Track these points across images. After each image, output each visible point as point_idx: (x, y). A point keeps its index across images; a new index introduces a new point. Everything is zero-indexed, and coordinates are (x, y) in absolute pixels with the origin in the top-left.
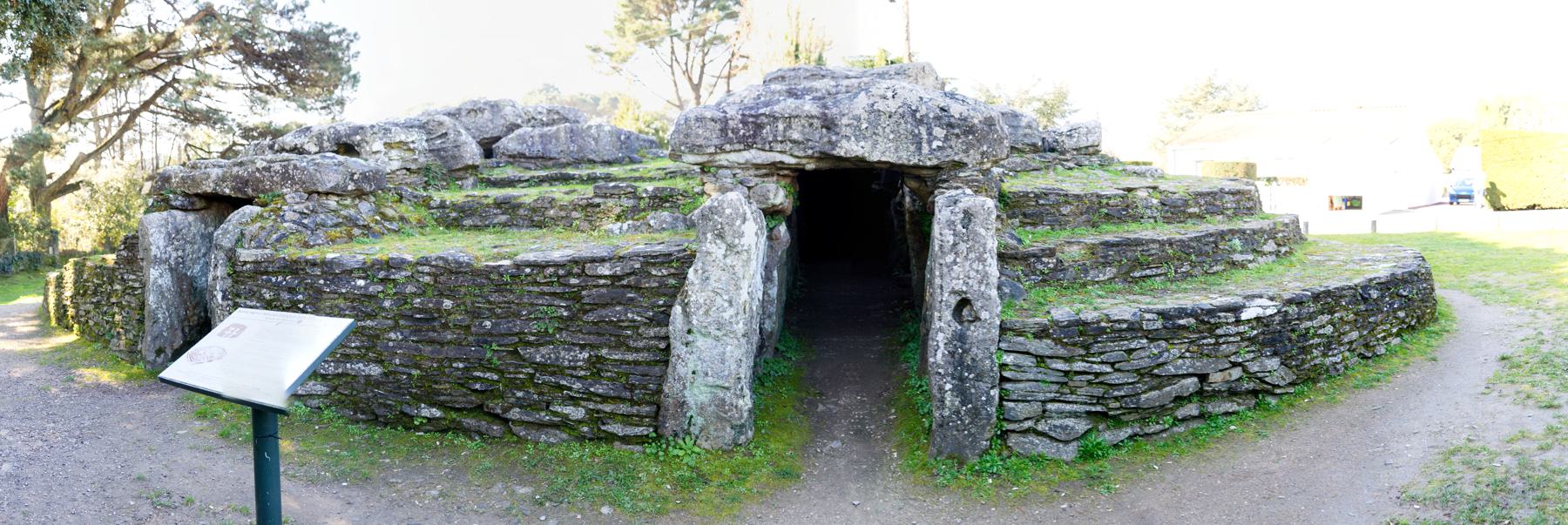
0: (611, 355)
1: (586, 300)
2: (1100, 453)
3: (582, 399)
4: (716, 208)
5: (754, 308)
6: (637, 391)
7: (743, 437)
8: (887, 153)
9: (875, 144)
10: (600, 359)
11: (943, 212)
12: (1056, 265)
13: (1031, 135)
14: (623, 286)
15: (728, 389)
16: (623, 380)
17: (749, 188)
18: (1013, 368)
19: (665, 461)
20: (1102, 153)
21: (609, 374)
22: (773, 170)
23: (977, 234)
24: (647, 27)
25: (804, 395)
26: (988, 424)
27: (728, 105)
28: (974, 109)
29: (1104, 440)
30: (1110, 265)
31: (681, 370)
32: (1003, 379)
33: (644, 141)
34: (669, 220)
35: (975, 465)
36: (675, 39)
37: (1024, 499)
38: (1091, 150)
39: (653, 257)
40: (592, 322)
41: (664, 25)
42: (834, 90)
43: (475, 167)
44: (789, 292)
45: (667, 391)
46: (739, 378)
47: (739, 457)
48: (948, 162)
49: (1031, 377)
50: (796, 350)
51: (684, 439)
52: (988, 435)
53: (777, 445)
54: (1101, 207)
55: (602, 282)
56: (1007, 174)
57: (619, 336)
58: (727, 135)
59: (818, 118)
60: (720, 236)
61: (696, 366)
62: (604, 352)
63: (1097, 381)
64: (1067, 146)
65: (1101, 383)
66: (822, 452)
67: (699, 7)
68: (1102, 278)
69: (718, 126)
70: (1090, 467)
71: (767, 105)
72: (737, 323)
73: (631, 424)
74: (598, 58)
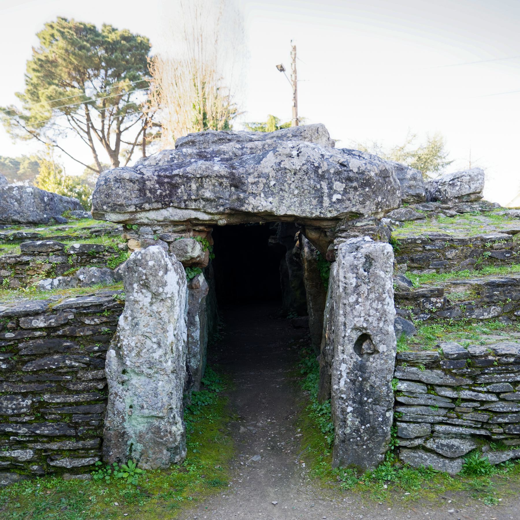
0: (53, 399)
1: (24, 352)
2: (483, 470)
3: (29, 441)
4: (140, 260)
5: (180, 348)
6: (81, 428)
7: (178, 457)
8: (293, 208)
9: (282, 199)
10: (42, 404)
11: (347, 258)
12: (443, 305)
13: (415, 187)
14: (59, 336)
15: (162, 418)
16: (67, 420)
17: (169, 243)
18: (406, 394)
19: (111, 483)
20: (483, 199)
21: (53, 416)
22: (190, 227)
23: (377, 276)
24: (60, 93)
25: (228, 420)
26: (384, 440)
27: (145, 167)
28: (371, 163)
29: (487, 460)
30: (494, 303)
31: (119, 405)
32: (398, 404)
33: (68, 202)
34: (97, 274)
35: (372, 473)
36: (90, 107)
37: (415, 503)
38: (473, 197)
39: (85, 308)
40: (32, 371)
41: (77, 92)
42: (240, 152)
44: (209, 334)
45: (108, 424)
46: (171, 408)
47: (175, 474)
48: (346, 213)
49: (422, 402)
50: (219, 384)
51: (127, 464)
52: (383, 450)
53: (207, 461)
54: (485, 250)
55: (38, 334)
56: (394, 224)
57: (60, 381)
58: (145, 194)
59: (227, 178)
60: (146, 286)
61: (132, 401)
62: (46, 397)
63: (482, 408)
64: (449, 195)
65: (486, 410)
66: (245, 464)
67: (111, 76)
68: (486, 316)
69: (136, 187)
70: (473, 481)
71: (180, 166)
72: (166, 362)
73: (78, 457)
74: (13, 122)
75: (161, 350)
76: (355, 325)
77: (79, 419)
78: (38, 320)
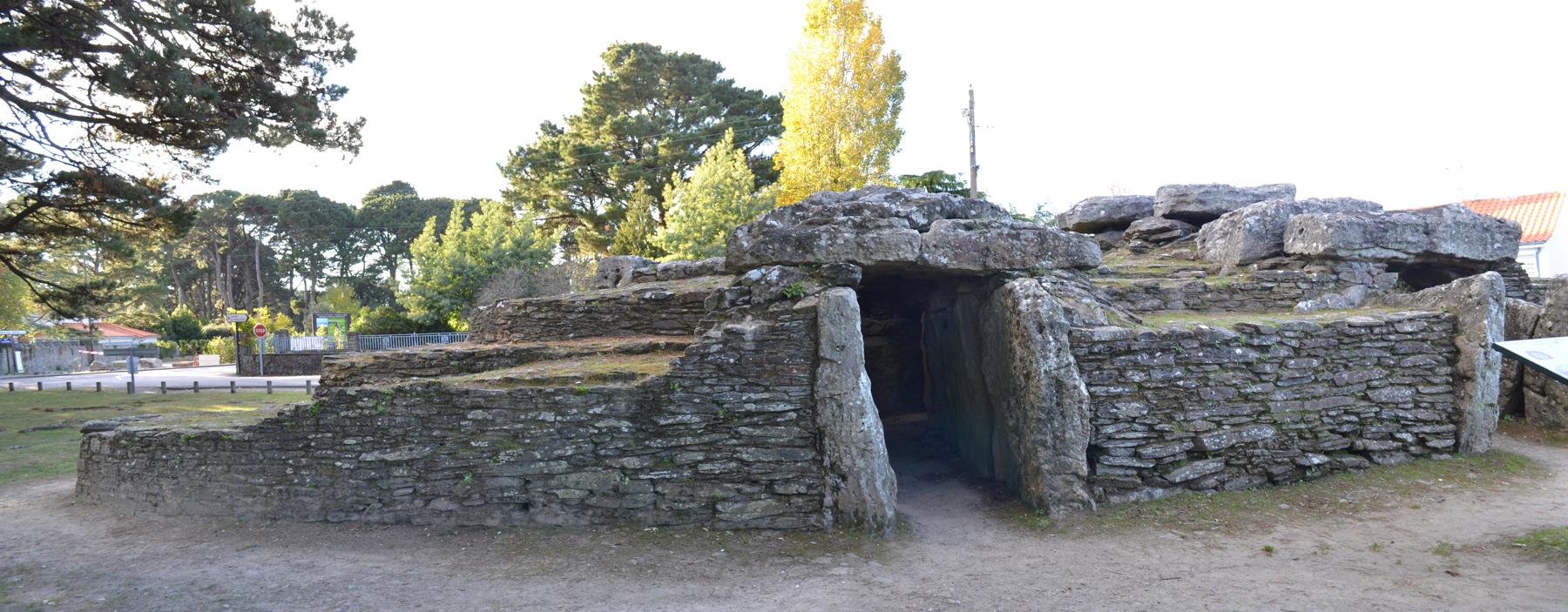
69: (1362, 229)
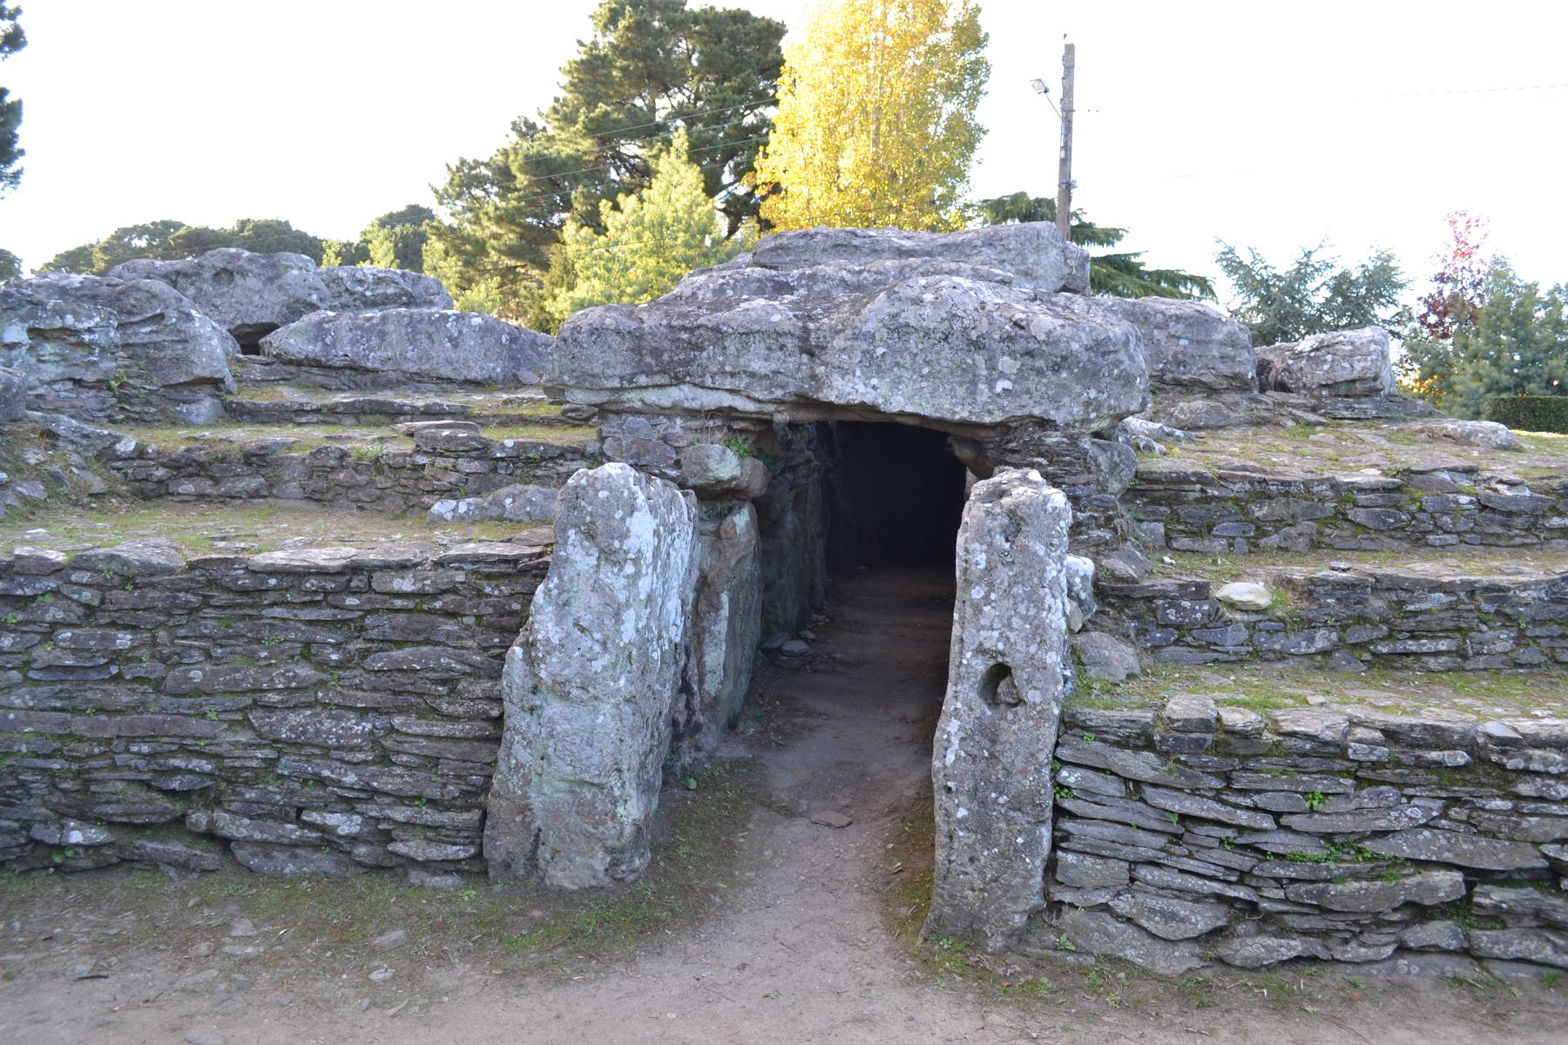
32: (1059, 812)
43: (215, 383)
49: (1113, 814)
55: (399, 603)
75: (607, 656)
76: (981, 644)
77: (450, 770)
78: (403, 578)
